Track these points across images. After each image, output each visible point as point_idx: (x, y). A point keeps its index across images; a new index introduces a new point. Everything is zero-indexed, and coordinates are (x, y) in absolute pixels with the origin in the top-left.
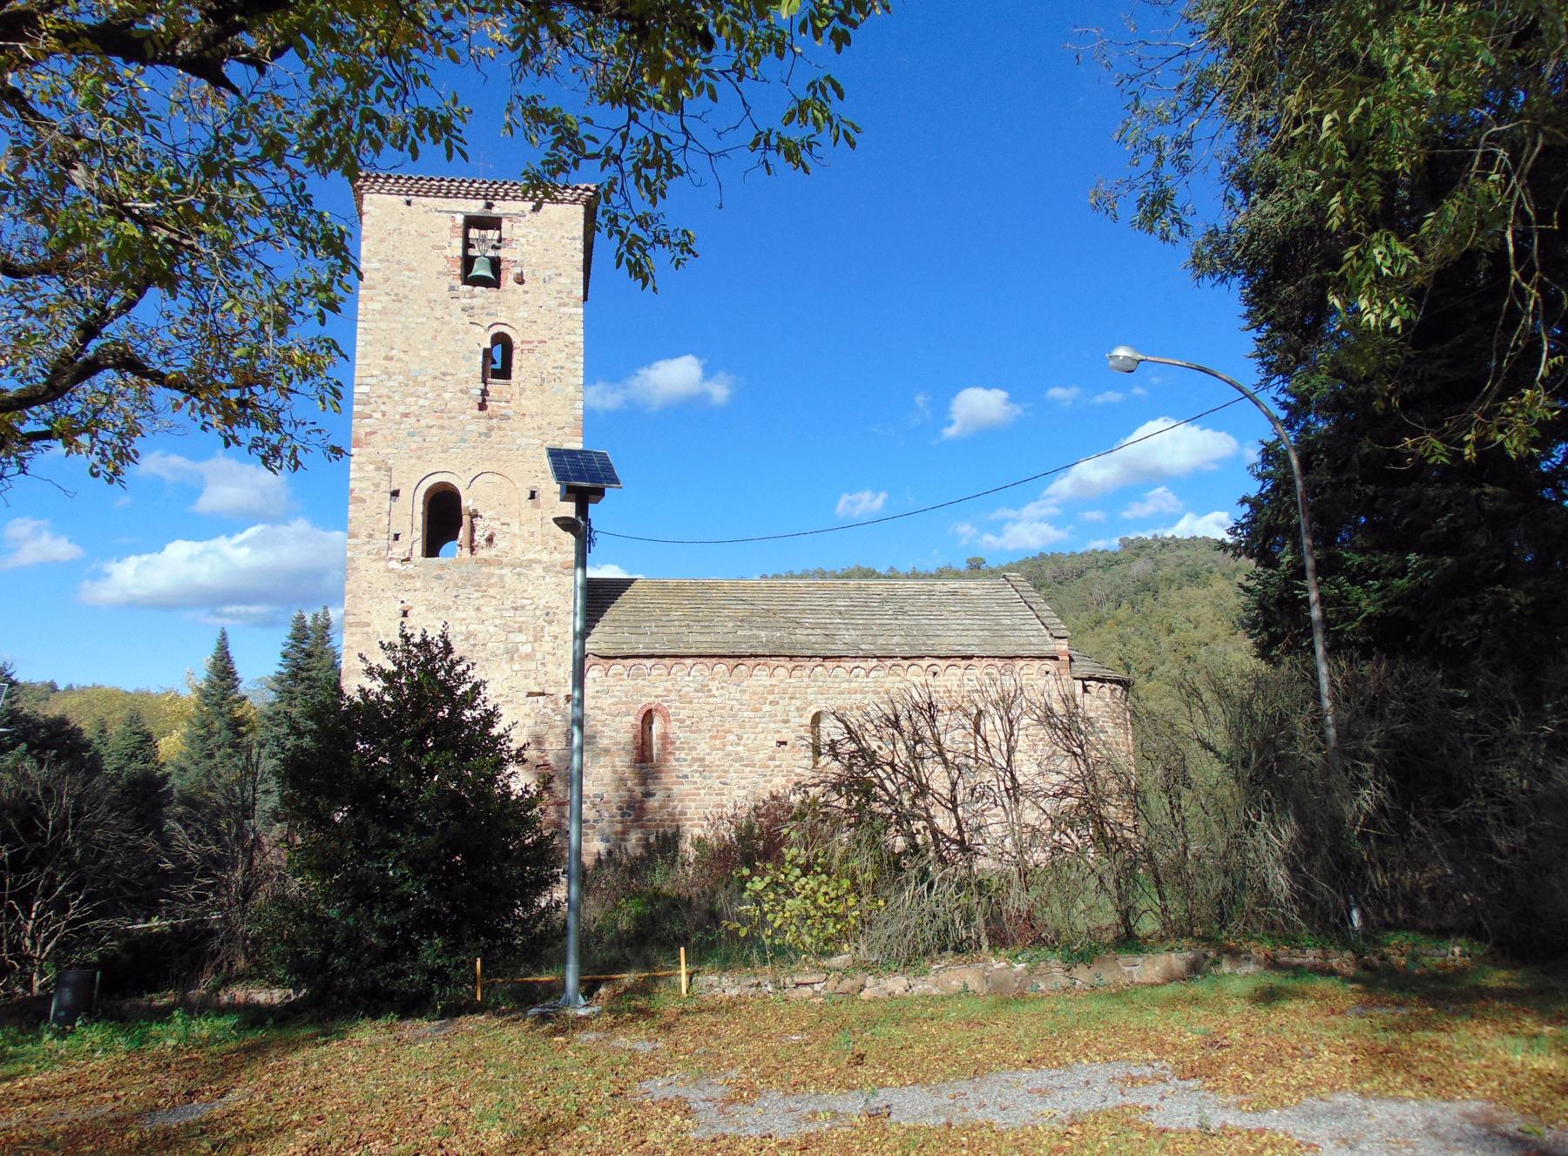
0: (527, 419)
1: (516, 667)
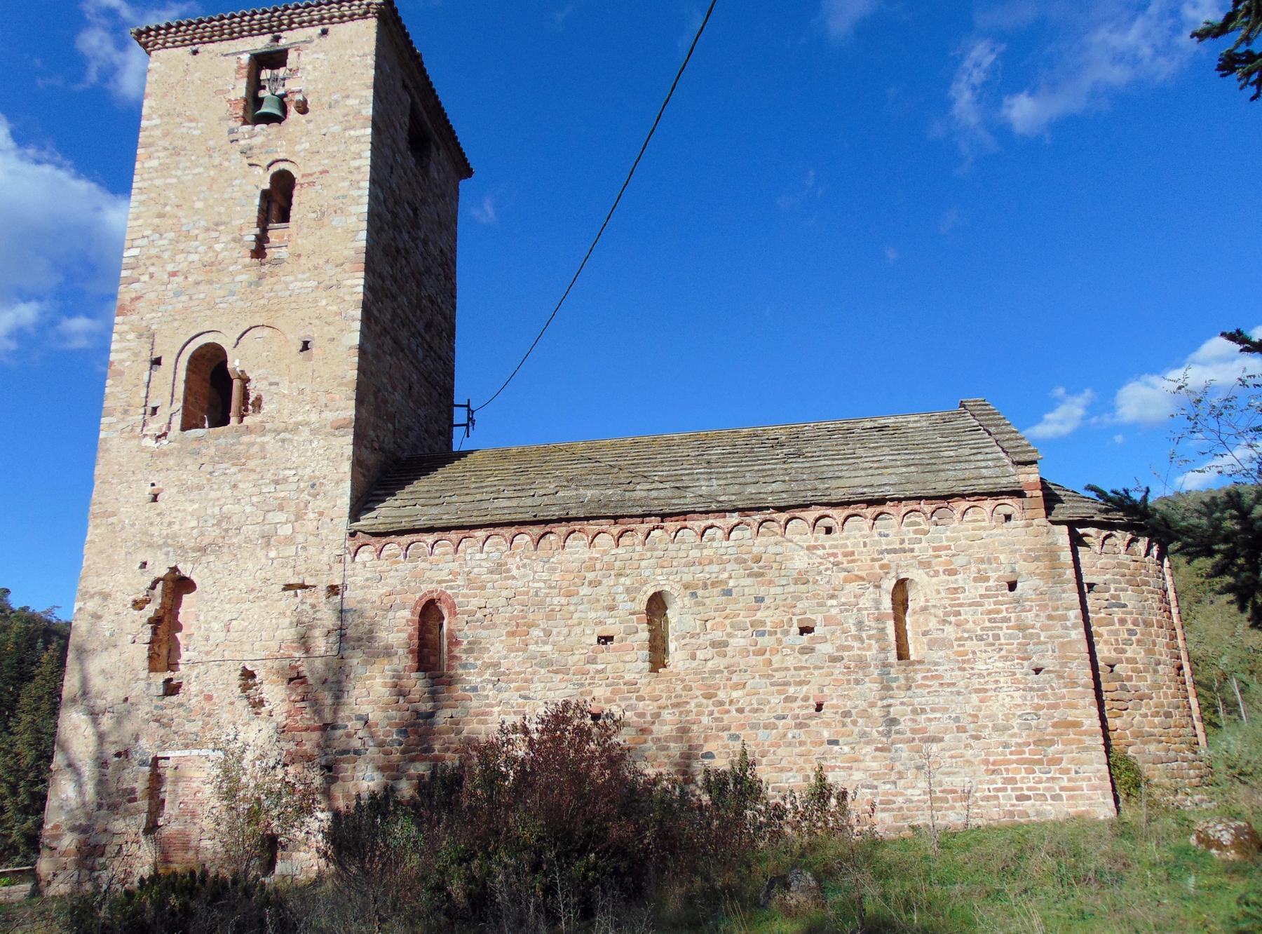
0: (303, 260)
1: (273, 554)
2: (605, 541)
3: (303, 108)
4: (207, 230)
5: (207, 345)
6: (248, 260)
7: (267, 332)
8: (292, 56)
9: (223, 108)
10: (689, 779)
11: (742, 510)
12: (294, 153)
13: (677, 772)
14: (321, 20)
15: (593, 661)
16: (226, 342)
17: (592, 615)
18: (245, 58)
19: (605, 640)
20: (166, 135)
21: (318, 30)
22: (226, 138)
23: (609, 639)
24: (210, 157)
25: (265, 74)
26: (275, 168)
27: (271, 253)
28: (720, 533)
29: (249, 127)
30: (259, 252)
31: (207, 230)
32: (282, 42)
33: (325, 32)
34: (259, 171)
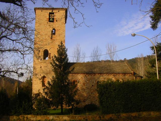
0: (57, 40)
2: (93, 76)
3: (57, 21)
4: (45, 35)
5: (45, 49)
6: (50, 39)
7: (53, 48)
8: (55, 13)
9: (46, 19)
10: (2, 90)
11: (106, 74)
12: (56, 26)
13: (22, 88)
14: (58, 10)
15: (91, 88)
16: (48, 49)
17: (91, 83)
18: (49, 13)
19: (93, 86)
20: (39, 22)
21: (58, 11)
22: (47, 23)
23: (93, 86)
24: (45, 25)
25: (51, 15)
26: (53, 28)
27: (53, 38)
28: (104, 76)
29: (50, 22)
30: (51, 39)
31: (45, 35)
32: (53, 12)
33: (59, 11)
34: (51, 28)
